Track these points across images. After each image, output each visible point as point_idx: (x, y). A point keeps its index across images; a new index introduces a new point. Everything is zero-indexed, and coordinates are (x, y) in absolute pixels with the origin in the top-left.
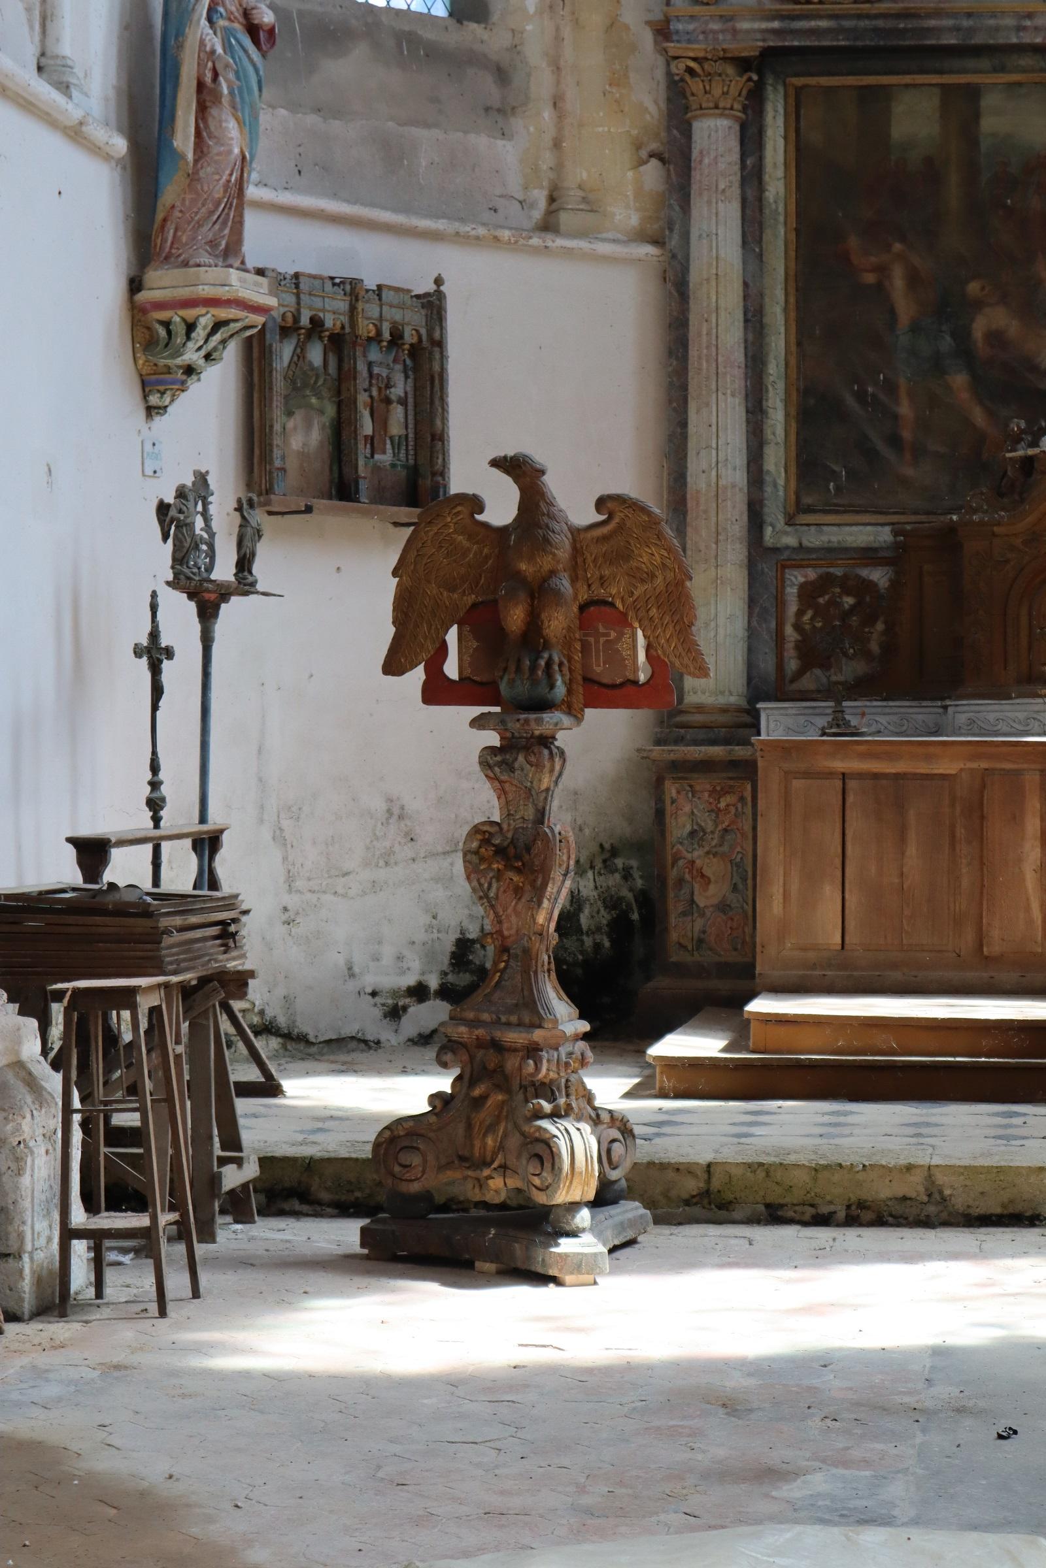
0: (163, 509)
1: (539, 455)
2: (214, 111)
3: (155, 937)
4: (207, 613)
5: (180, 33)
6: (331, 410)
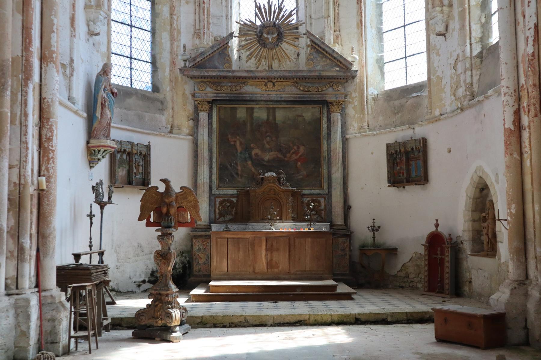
0: (93, 187)
1: (169, 179)
3: (90, 274)
4: (102, 208)
5: (98, 93)
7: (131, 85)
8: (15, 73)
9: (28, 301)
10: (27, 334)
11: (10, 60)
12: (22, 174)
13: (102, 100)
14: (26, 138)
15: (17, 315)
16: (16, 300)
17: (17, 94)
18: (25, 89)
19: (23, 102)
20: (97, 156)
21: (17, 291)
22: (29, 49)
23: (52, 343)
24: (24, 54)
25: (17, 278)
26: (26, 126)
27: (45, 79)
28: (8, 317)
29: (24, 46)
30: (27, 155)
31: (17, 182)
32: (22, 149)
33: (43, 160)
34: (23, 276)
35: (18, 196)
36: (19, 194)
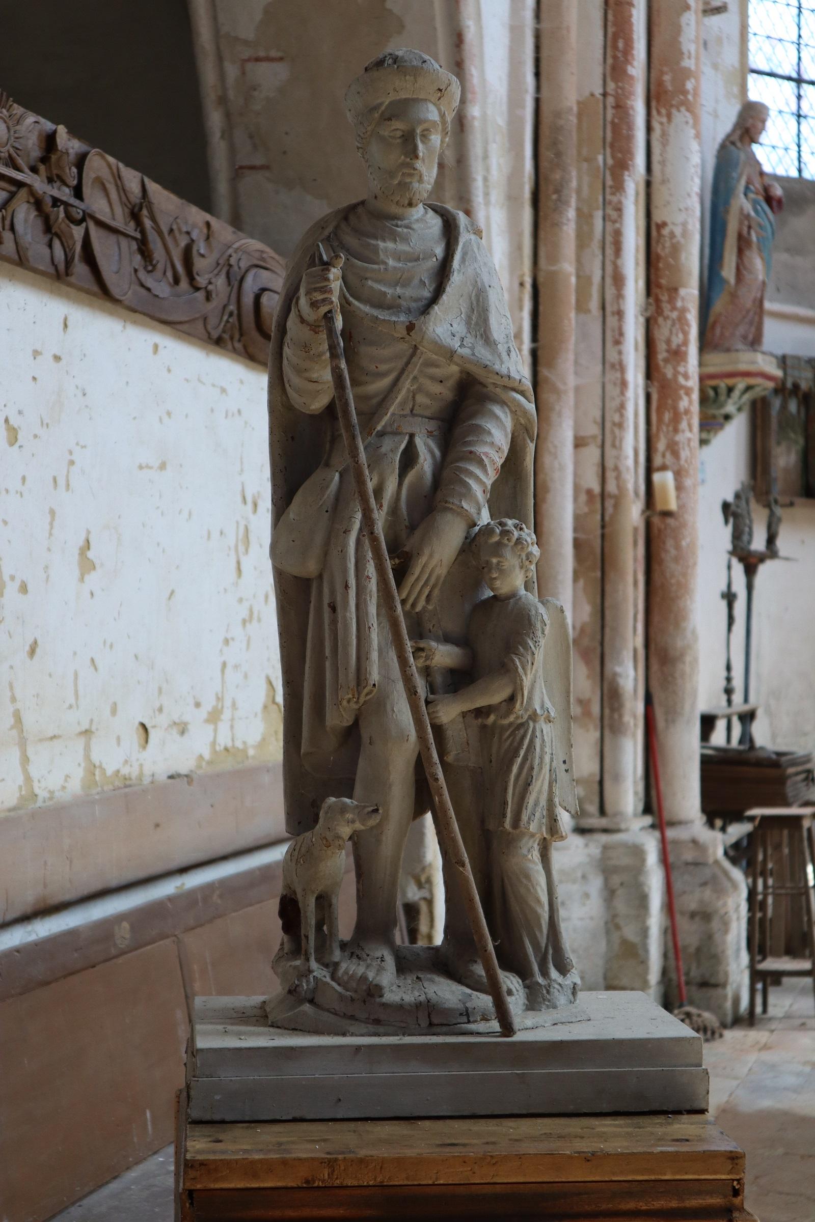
0: (726, 506)
2: (747, 253)
3: (782, 780)
4: (750, 571)
5: (727, 203)
6: (801, 441)
7: (800, 171)
8: (585, 152)
9: (638, 852)
10: (641, 952)
11: (575, 109)
12: (610, 464)
13: (741, 223)
14: (620, 353)
15: (610, 894)
16: (606, 848)
17: (591, 216)
18: (614, 199)
19: (609, 239)
20: (722, 406)
21: (603, 822)
22: (625, 72)
23: (705, 984)
24: (611, 86)
25: (601, 783)
26: (620, 314)
27: (663, 163)
28: (587, 896)
29: (610, 61)
30: (622, 407)
31: (597, 489)
32: (609, 387)
33: (660, 420)
34: (617, 778)
35: (599, 532)
36: (603, 527)
